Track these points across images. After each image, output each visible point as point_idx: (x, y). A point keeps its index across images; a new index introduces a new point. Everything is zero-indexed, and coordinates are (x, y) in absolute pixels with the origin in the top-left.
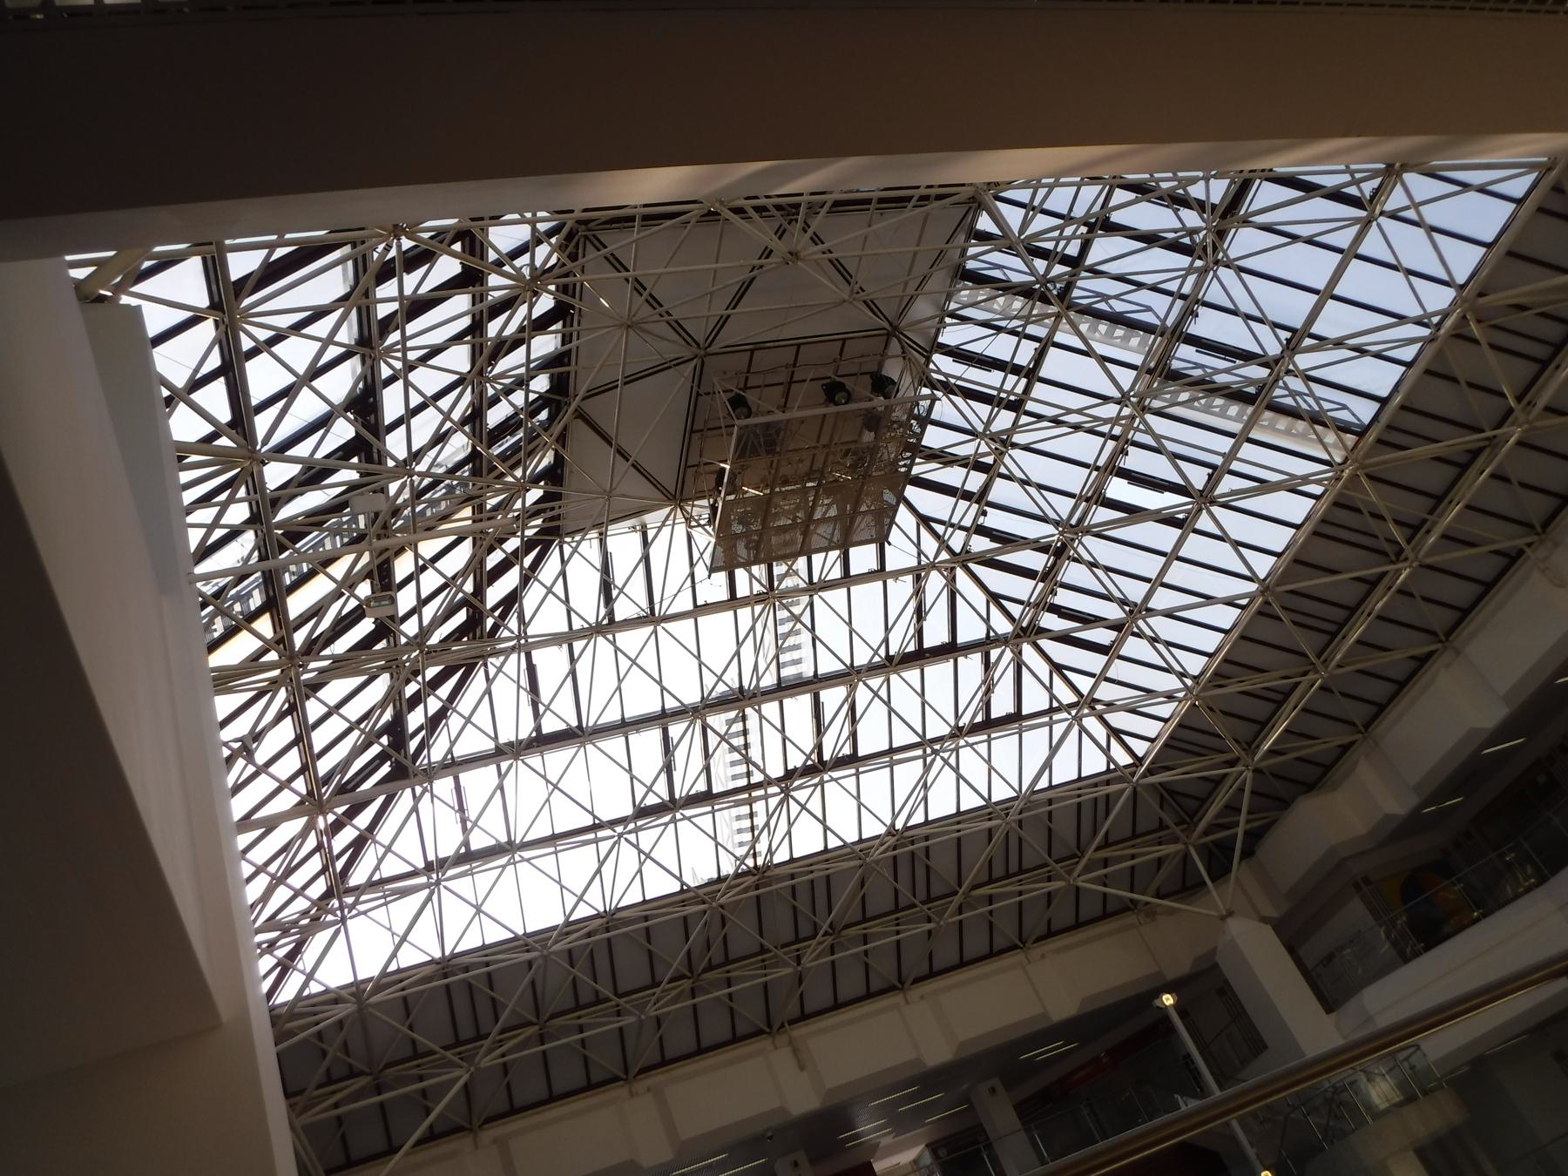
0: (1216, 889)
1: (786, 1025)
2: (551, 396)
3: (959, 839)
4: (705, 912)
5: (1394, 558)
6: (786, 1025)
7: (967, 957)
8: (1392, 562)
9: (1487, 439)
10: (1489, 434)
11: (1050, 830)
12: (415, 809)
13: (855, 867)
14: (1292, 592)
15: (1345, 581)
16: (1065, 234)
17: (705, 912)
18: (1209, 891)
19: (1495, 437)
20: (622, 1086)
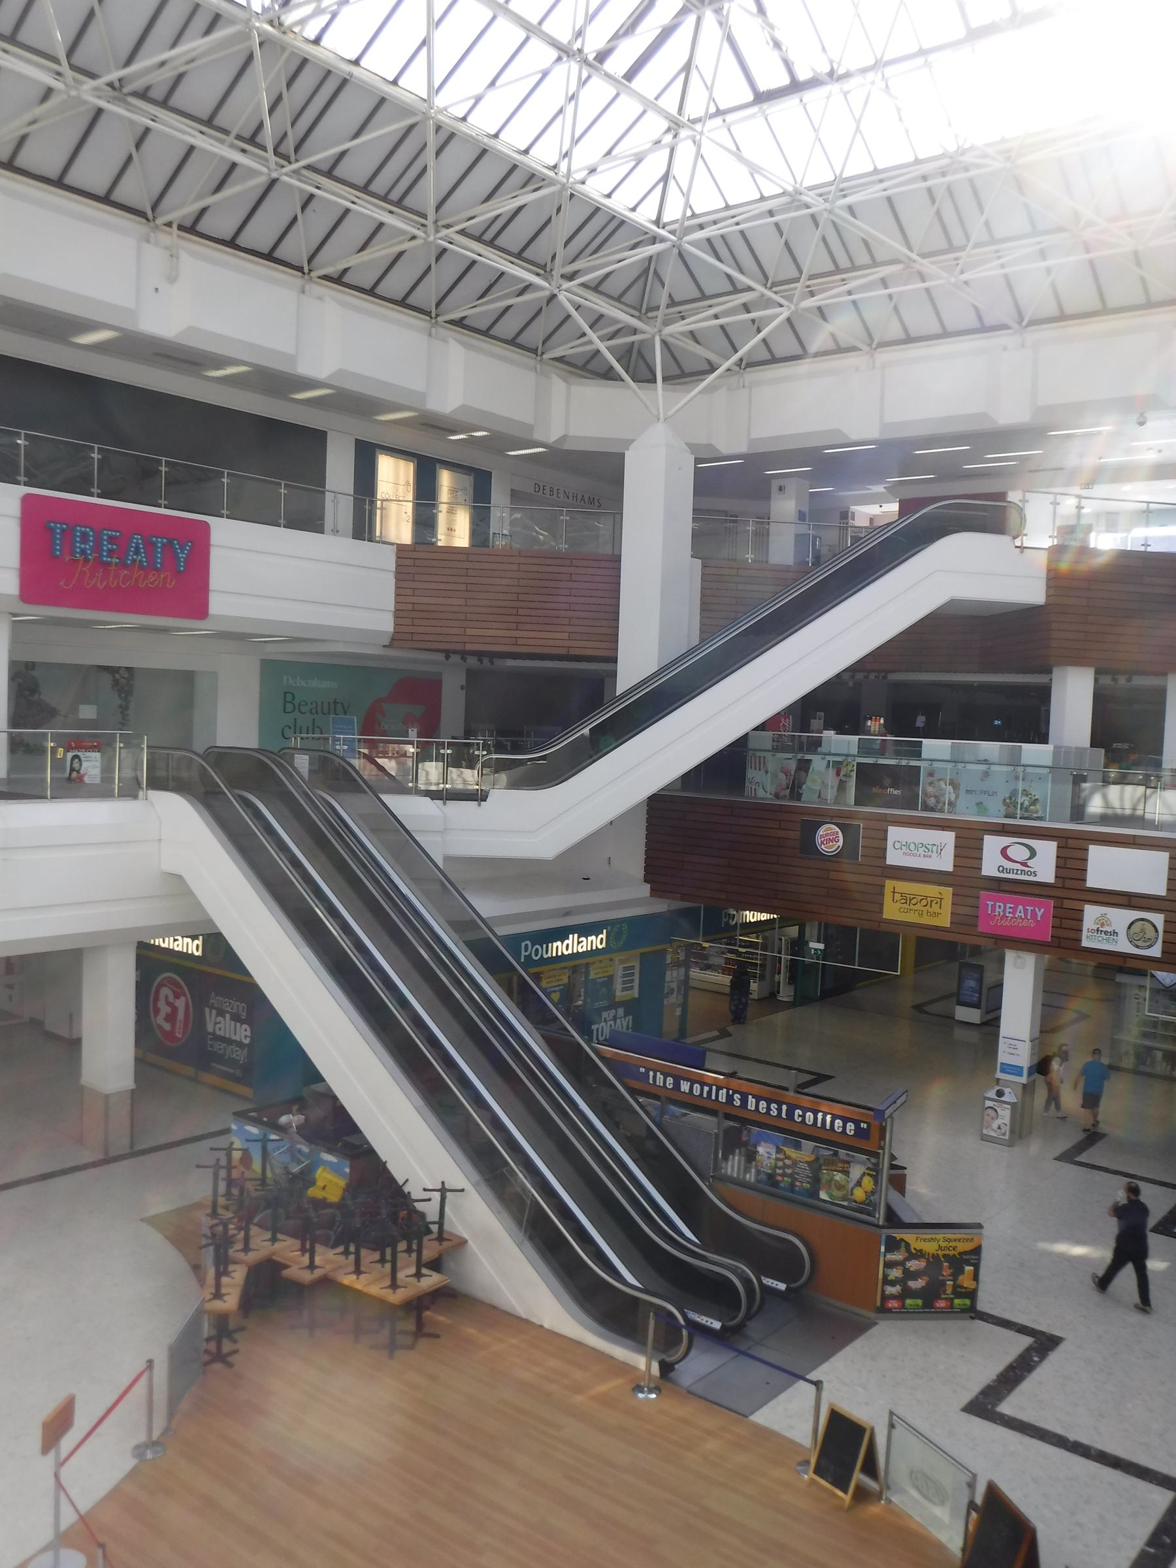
0: (664, 390)
1: (175, 226)
2: (524, 1226)
3: (474, 262)
4: (414, 238)
5: (769, 285)
6: (175, 226)
7: (410, 301)
8: (765, 286)
9: (909, 258)
10: (914, 256)
11: (138, 146)
12: (699, 155)
13: (404, 232)
14: (719, 259)
15: (721, 270)
16: (908, 1264)
17: (414, 238)
18: (656, 389)
19: (914, 261)
20: (426, 320)
